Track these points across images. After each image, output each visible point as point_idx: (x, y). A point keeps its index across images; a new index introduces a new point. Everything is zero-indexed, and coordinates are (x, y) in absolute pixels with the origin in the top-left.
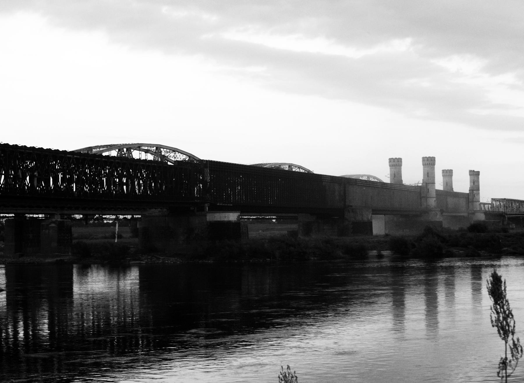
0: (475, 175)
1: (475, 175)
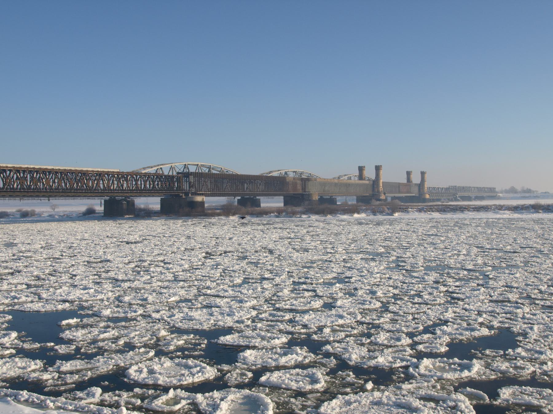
0: (423, 174)
1: (423, 174)
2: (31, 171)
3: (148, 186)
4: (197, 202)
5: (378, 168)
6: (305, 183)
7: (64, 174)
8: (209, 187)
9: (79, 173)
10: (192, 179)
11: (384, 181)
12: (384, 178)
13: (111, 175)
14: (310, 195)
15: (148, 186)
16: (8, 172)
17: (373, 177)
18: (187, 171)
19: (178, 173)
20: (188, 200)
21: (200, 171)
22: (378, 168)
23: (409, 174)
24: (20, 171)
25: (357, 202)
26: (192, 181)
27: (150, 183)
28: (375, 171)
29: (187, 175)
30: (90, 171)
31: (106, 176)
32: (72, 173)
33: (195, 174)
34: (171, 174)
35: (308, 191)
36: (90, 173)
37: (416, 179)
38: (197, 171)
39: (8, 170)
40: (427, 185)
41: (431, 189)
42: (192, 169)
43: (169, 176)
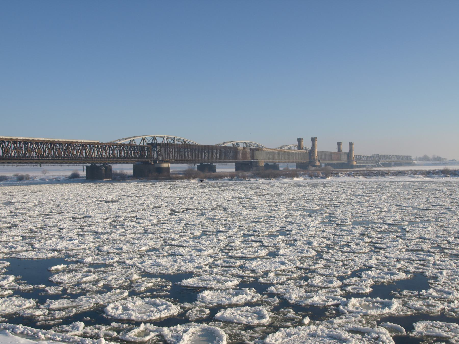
0: (351, 144)
1: (351, 144)
2: (25, 142)
3: (123, 154)
4: (164, 168)
5: (314, 140)
6: (253, 152)
7: (53, 144)
8: (174, 156)
9: (65, 144)
10: (159, 148)
11: (319, 150)
12: (319, 148)
13: (92, 146)
14: (257, 162)
15: (123, 154)
16: (7, 143)
17: (310, 147)
18: (155, 142)
19: (148, 144)
20: (156, 166)
21: (166, 142)
22: (314, 140)
23: (339, 144)
24: (16, 142)
25: (296, 168)
26: (160, 150)
27: (124, 152)
28: (311, 142)
29: (155, 145)
30: (75, 142)
31: (88, 146)
32: (60, 144)
33: (162, 145)
34: (142, 144)
35: (255, 158)
36: (74, 144)
37: (345, 149)
38: (164, 142)
39: (7, 141)
40: (354, 154)
41: (358, 157)
42: (160, 141)
43: (140, 146)
